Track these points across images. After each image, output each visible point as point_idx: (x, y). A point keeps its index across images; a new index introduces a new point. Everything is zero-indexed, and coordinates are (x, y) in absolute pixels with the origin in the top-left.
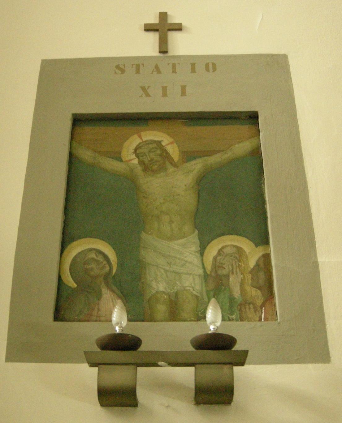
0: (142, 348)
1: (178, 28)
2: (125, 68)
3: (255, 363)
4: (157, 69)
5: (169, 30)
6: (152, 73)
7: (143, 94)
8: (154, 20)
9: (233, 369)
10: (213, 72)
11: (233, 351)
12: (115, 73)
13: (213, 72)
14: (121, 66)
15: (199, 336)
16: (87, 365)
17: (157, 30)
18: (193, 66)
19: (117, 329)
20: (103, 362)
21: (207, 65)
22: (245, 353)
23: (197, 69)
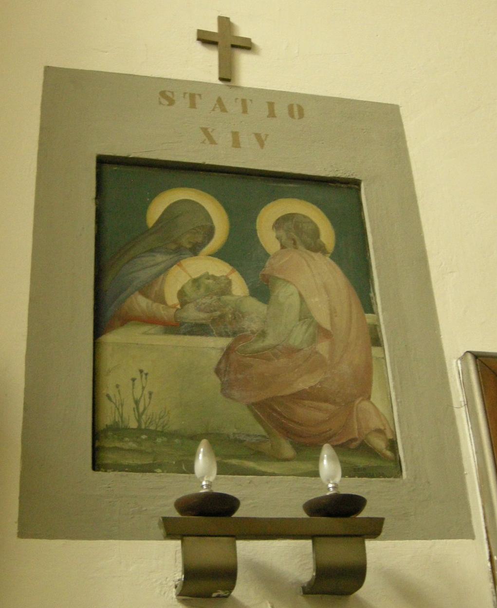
0: (364, 514)
1: (247, 46)
2: (159, 99)
5: (233, 46)
7: (205, 140)
8: (213, 27)
9: (364, 543)
10: (299, 119)
11: (232, 518)
12: (160, 103)
13: (299, 119)
14: (167, 103)
18: (271, 105)
21: (291, 108)
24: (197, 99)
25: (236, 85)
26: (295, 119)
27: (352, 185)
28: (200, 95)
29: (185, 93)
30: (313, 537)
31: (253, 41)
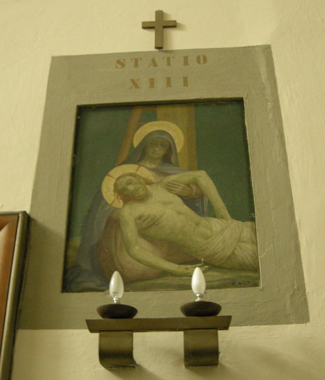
0: (137, 316)
1: (174, 25)
2: (125, 62)
3: (236, 325)
4: (154, 63)
5: (165, 27)
6: (149, 66)
12: (124, 60)
15: (190, 304)
16: (87, 331)
17: (159, 48)
18: (186, 58)
19: (115, 301)
20: (114, 332)
21: (198, 58)
22: (229, 318)
23: (189, 62)
24: (140, 62)
25: (169, 49)
26: (201, 64)
27: (239, 102)
28: (141, 59)
29: (164, 58)
30: (184, 330)
31: (178, 21)
